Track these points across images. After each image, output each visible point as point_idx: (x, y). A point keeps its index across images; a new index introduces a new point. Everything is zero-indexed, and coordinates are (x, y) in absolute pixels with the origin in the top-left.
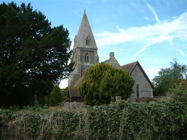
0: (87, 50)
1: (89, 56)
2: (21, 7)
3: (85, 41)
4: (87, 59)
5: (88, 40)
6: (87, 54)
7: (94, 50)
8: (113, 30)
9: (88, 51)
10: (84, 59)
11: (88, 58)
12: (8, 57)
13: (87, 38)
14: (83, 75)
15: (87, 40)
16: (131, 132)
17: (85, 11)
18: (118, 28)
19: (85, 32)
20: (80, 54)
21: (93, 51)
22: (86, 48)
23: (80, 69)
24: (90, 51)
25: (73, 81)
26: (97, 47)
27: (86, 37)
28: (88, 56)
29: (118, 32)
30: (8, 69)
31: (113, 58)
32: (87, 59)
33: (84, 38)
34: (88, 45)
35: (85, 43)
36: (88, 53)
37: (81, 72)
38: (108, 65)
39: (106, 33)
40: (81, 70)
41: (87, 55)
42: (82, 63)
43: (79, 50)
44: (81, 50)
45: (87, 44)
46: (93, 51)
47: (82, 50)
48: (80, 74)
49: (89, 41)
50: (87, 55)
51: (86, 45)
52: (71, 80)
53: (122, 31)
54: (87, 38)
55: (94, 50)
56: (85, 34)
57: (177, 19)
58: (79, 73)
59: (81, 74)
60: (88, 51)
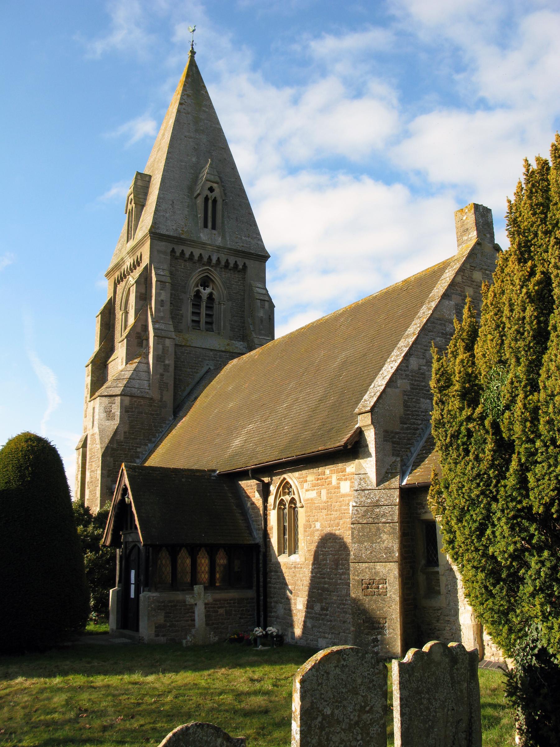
0: (205, 259)
1: (216, 295)
2: (436, 570)
3: (200, 201)
4: (203, 311)
5: (215, 201)
6: (205, 282)
7: (251, 264)
9: (214, 261)
10: (187, 309)
11: (209, 308)
13: (211, 190)
14: (221, 216)
15: (207, 199)
17: (193, 53)
20: (167, 273)
21: (245, 266)
22: (203, 245)
23: (166, 368)
25: (121, 437)
27: (207, 180)
28: (210, 297)
31: (488, 247)
32: (203, 311)
34: (214, 228)
35: (201, 215)
36: (216, 276)
37: (171, 383)
40: (172, 369)
41: (208, 290)
42: (177, 330)
43: (159, 252)
44: (173, 251)
46: (245, 266)
47: (178, 254)
48: (168, 397)
50: (208, 290)
51: (206, 226)
52: (110, 434)
54: (211, 190)
55: (247, 262)
56: (197, 170)
58: (162, 386)
59: (175, 399)
60: (214, 261)
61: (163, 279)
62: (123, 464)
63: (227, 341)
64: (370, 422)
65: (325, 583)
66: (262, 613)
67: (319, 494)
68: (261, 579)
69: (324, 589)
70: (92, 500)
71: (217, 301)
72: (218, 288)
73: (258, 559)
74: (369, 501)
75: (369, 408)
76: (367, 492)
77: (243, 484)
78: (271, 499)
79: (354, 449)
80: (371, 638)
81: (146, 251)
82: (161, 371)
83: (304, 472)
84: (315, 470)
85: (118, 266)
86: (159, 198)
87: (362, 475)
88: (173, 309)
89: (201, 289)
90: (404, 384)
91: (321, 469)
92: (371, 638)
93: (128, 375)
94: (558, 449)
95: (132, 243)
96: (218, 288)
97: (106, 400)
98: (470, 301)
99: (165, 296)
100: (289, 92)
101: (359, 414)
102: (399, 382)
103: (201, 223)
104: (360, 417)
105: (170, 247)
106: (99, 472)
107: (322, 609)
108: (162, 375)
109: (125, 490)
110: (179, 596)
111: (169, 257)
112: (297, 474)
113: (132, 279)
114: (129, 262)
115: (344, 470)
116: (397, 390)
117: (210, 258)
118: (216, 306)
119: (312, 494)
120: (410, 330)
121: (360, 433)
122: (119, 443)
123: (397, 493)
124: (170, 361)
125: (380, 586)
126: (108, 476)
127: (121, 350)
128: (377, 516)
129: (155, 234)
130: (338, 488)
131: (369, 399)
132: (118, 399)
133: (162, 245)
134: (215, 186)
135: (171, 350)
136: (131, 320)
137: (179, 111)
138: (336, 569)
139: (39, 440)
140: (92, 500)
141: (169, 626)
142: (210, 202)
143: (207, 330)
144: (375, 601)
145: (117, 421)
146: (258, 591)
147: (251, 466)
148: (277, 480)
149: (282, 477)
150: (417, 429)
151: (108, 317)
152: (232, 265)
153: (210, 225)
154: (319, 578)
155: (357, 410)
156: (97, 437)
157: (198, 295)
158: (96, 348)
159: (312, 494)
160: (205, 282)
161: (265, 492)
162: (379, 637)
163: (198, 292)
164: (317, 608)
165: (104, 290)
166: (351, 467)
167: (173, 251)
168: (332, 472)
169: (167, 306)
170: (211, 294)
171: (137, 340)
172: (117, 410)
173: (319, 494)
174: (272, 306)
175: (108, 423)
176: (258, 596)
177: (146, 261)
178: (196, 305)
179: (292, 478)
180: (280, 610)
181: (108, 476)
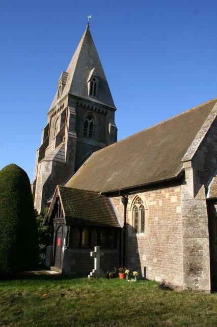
0: (90, 108)
1: (94, 123)
5: (95, 85)
6: (90, 117)
7: (109, 112)
10: (82, 128)
11: (91, 128)
23: (72, 151)
28: (92, 124)
34: (94, 95)
36: (95, 116)
37: (74, 157)
40: (75, 152)
41: (91, 121)
43: (71, 102)
44: (77, 103)
48: (73, 163)
50: (91, 121)
61: (73, 114)
62: (57, 186)
63: (97, 143)
64: (191, 166)
65: (160, 248)
66: (122, 261)
67: (158, 203)
68: (122, 245)
69: (159, 251)
70: (37, 206)
71: (94, 125)
72: (95, 121)
73: (121, 235)
74: (191, 206)
75: (191, 159)
76: (189, 201)
77: (112, 199)
78: (129, 206)
79: (180, 180)
80: (193, 279)
81: (66, 102)
82: (70, 152)
83: (148, 192)
84: (155, 191)
85: (53, 110)
86: (73, 81)
87: (186, 194)
88: (75, 127)
89: (88, 120)
90: (205, 149)
91: (158, 191)
92: (193, 279)
93: (56, 153)
95: (60, 100)
96: (95, 121)
97: (46, 163)
99: (74, 121)
101: (184, 162)
102: (203, 148)
104: (184, 164)
106: (41, 194)
107: (158, 261)
108: (70, 154)
109: (58, 198)
110: (83, 252)
112: (145, 193)
113: (59, 114)
114: (58, 107)
115: (173, 191)
116: (202, 151)
118: (94, 128)
119: (154, 203)
120: (205, 124)
121: (183, 172)
122: (51, 181)
123: (205, 202)
124: (74, 148)
125: (199, 251)
126: (45, 196)
127: (52, 142)
128: (196, 213)
129: (70, 96)
130: (169, 200)
131: (190, 153)
132: (51, 163)
134: (96, 78)
135: (75, 143)
136: (59, 130)
137: (82, 48)
138: (167, 241)
139: (19, 168)
140: (37, 206)
141: (108, 274)
143: (90, 137)
144: (197, 259)
145: (50, 172)
146: (120, 250)
147: (120, 188)
148: (133, 196)
149: (136, 195)
150: (210, 172)
151: (47, 130)
152: (101, 111)
154: (156, 245)
155: (182, 160)
156: (41, 179)
157: (86, 123)
158: (42, 143)
159: (154, 203)
161: (125, 202)
162: (199, 278)
163: (87, 121)
166: (177, 189)
167: (77, 103)
168: (166, 192)
169: (74, 125)
170: (92, 122)
171: (60, 138)
172: (50, 167)
173: (158, 203)
174: (117, 130)
175: (47, 173)
176: (120, 253)
177: (66, 105)
178: (86, 127)
179: (142, 195)
180: (133, 260)
181: (45, 196)
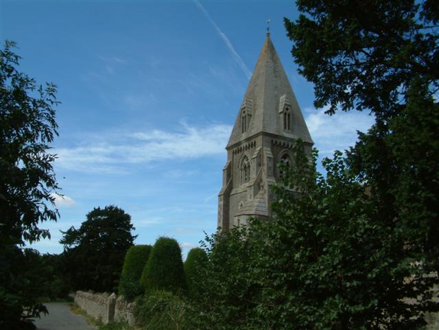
0: (286, 145)
3: (282, 115)
8: (172, 126)
12: (346, 20)
16: (419, 265)
18: (184, 123)
19: (276, 92)
22: (285, 138)
24: (284, 144)
26: (310, 138)
29: (185, 133)
30: (358, 199)
33: (277, 109)
34: (289, 129)
38: (48, 219)
39: (157, 133)
41: (286, 161)
43: (266, 141)
44: (272, 141)
45: (288, 125)
47: (274, 142)
49: (291, 117)
50: (286, 161)
51: (285, 128)
53: (193, 130)
56: (277, 97)
57: (316, 113)
94: (437, 88)
98: (346, 54)
100: (299, 19)
103: (283, 126)
105: (271, 139)
111: (270, 145)
117: (288, 145)
133: (268, 138)
142: (287, 116)
153: (287, 128)
160: (285, 157)
164: (51, 268)
165: (240, 92)
